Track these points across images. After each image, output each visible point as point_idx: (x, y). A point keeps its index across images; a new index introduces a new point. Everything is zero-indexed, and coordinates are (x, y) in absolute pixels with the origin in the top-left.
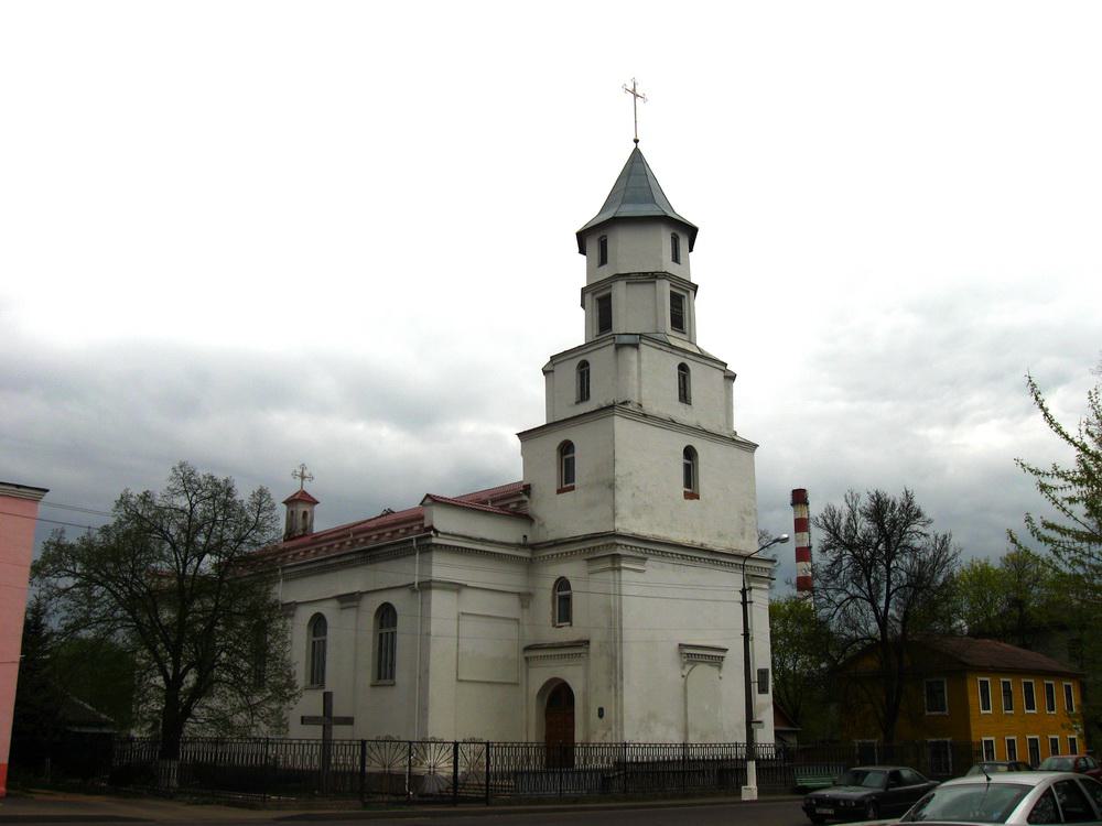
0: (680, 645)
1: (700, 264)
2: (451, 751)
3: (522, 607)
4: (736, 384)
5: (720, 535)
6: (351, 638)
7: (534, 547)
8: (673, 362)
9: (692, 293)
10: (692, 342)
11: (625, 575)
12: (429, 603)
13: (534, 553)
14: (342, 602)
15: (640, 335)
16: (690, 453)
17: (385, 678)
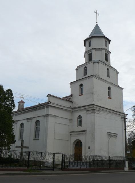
1: (111, 47)
2: (53, 155)
3: (70, 122)
4: (119, 75)
5: (116, 108)
6: (29, 128)
7: (73, 108)
8: (106, 67)
10: (110, 64)
11: (96, 114)
12: (48, 120)
13: (73, 110)
14: (27, 120)
16: (109, 88)
17: (37, 138)
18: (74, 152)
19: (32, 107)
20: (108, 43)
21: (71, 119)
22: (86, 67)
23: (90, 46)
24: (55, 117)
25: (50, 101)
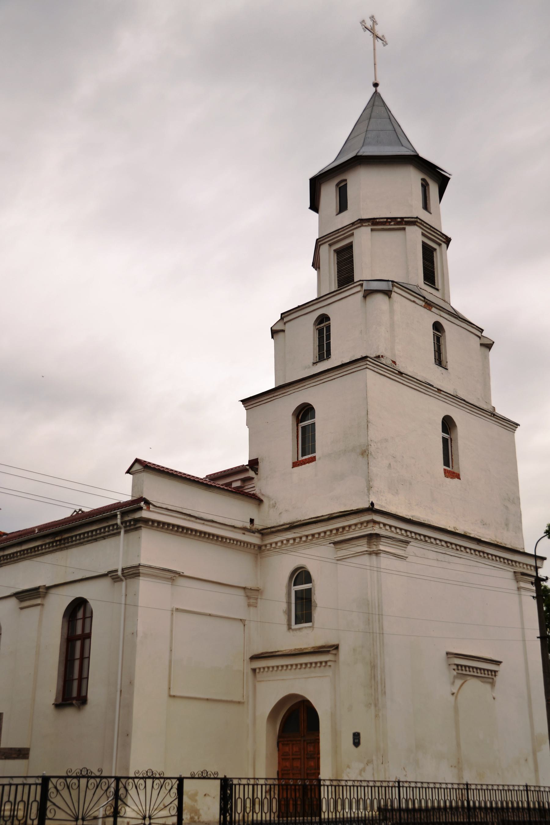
0: (448, 653)
2: (175, 790)
3: (249, 605)
7: (264, 532)
9: (444, 246)
11: (385, 561)
12: (136, 594)
15: (393, 281)
18: (276, 769)
19: (42, 528)
20: (434, 189)
21: (258, 590)
22: (323, 319)
23: (343, 206)
24: (172, 580)
25: (145, 496)
